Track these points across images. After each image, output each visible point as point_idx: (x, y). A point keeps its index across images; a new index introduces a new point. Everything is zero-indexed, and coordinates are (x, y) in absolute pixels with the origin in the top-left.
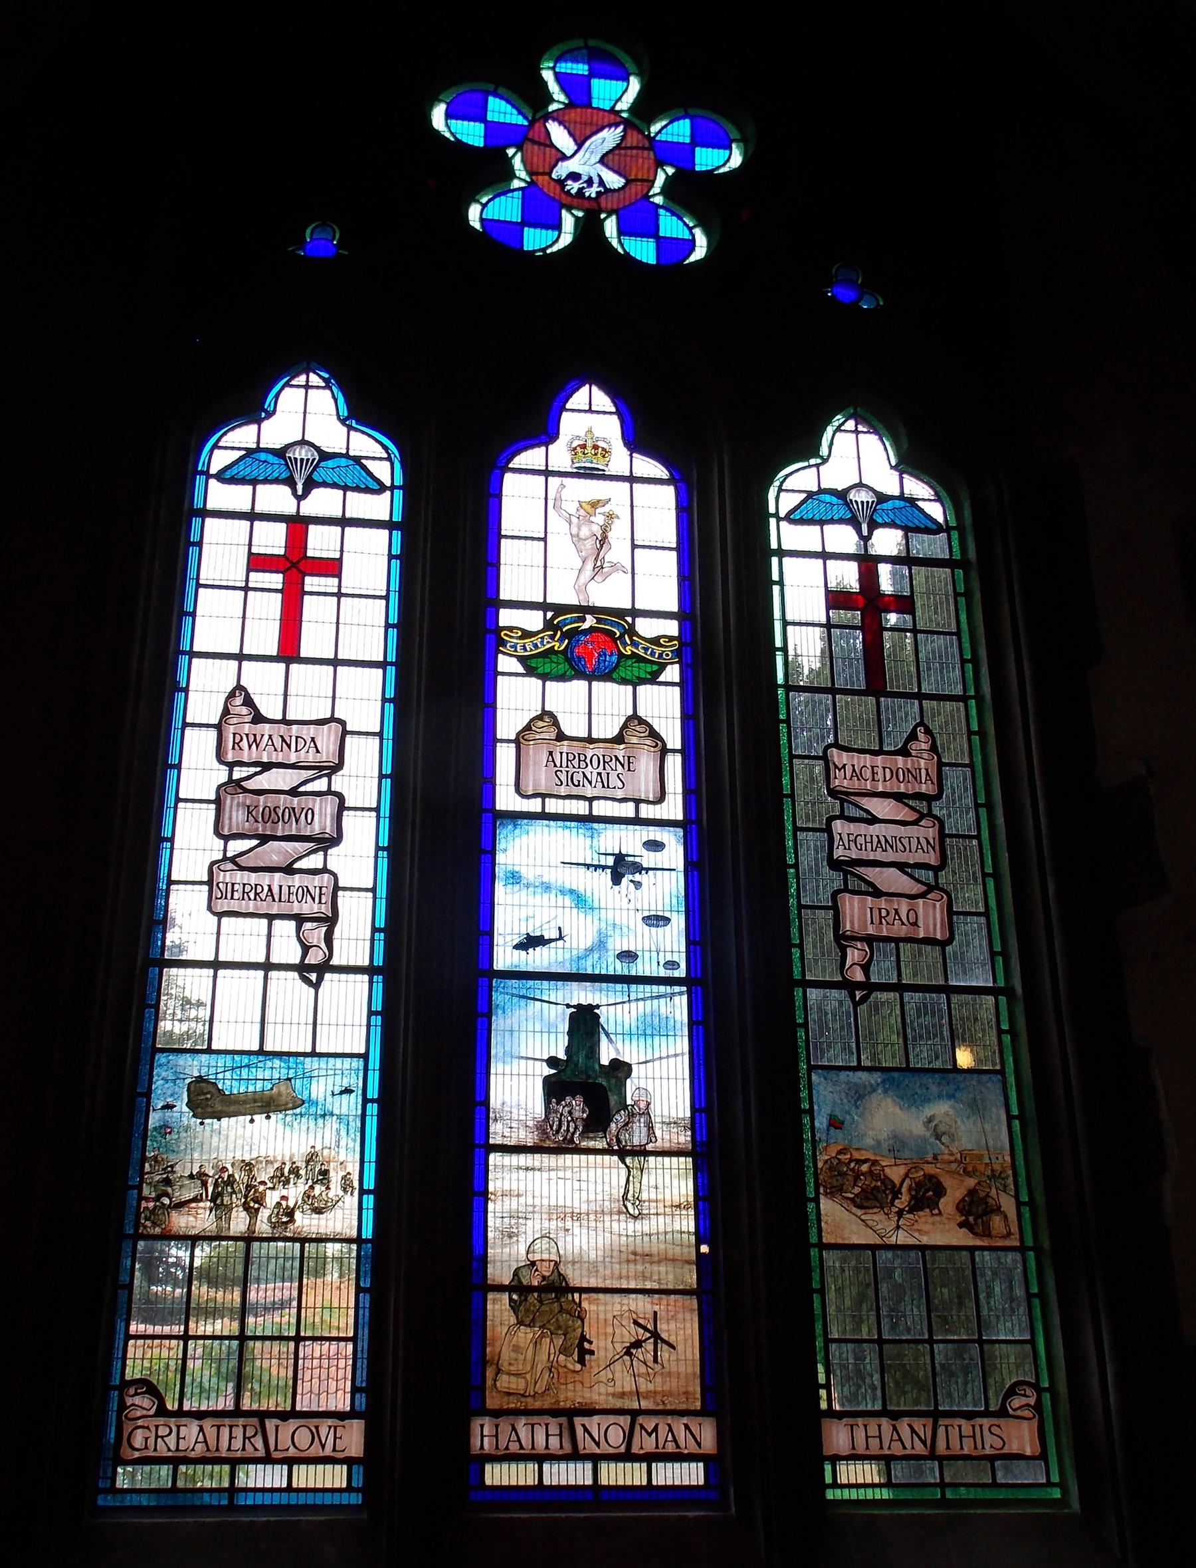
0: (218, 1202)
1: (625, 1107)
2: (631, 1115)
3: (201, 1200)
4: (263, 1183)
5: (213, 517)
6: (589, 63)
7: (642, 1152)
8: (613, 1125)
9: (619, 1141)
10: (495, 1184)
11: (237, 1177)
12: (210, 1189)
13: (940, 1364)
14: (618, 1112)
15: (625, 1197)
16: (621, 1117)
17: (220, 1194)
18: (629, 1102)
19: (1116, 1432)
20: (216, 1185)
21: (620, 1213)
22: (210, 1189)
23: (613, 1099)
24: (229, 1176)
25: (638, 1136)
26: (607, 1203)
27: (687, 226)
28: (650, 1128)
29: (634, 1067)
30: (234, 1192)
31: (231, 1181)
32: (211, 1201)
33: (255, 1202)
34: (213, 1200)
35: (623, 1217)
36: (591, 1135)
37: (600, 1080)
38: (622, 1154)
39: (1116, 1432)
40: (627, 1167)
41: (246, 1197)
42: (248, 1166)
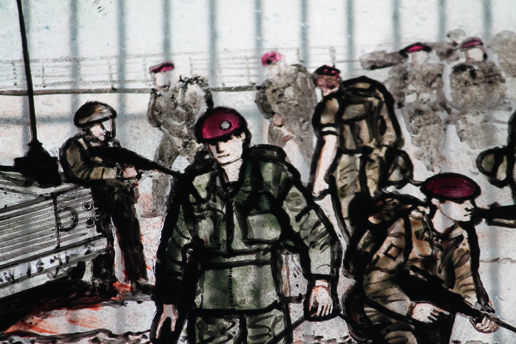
0: (204, 297)
3: (105, 293)
4: (447, 186)
5: (36, 136)
6: (88, 149)
10: (164, 308)
11: (295, 156)
12: (151, 233)
17: (211, 258)
20: (181, 203)
22: (151, 233)
24: (253, 157)
27: (148, 56)
30: (293, 242)
31: (265, 183)
32: (160, 295)
33: (417, 293)
34: (174, 287)
41: (359, 263)
42: (355, 104)
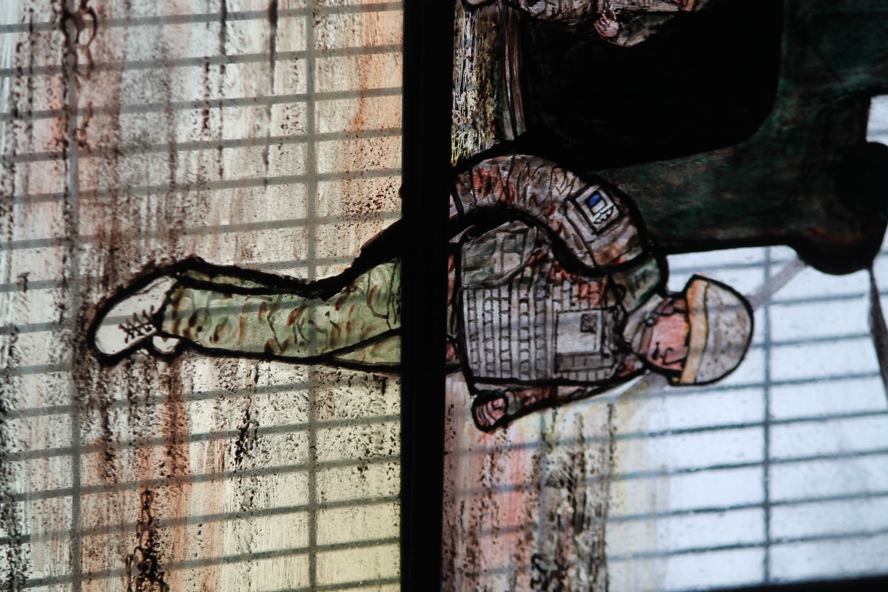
1: (657, 244)
2: (612, 280)
7: (426, 352)
8: (562, 185)
9: (483, 221)
13: (645, 271)
14: (629, 208)
15: (190, 272)
16: (593, 223)
18: (682, 265)
19: (507, 62)
21: (113, 245)
23: (691, 177)
25: (499, 327)
26: (156, 171)
28: (549, 390)
29: (858, 280)
35: (90, 262)
36: (511, 70)
37: (786, 111)
38: (425, 242)
39: (507, 62)
40: (348, 279)
